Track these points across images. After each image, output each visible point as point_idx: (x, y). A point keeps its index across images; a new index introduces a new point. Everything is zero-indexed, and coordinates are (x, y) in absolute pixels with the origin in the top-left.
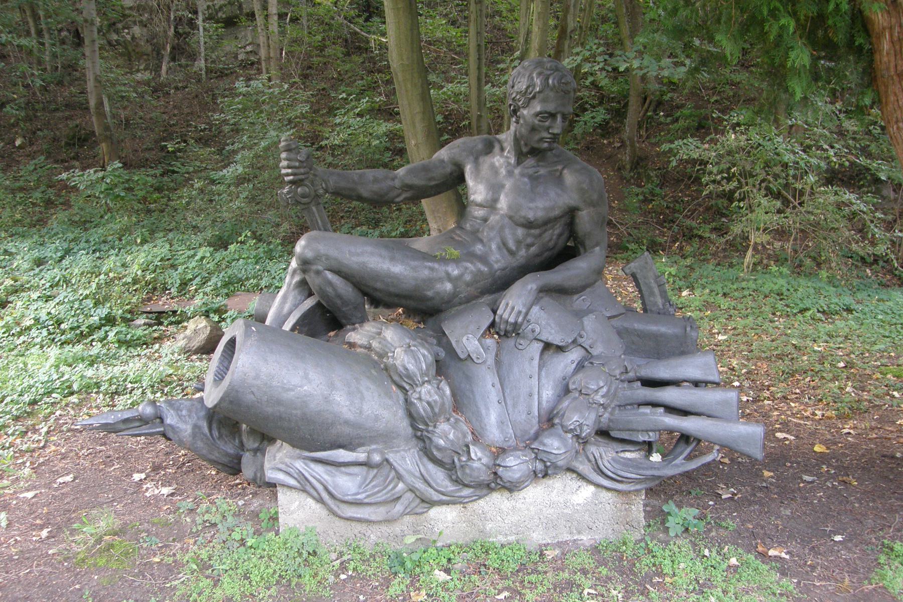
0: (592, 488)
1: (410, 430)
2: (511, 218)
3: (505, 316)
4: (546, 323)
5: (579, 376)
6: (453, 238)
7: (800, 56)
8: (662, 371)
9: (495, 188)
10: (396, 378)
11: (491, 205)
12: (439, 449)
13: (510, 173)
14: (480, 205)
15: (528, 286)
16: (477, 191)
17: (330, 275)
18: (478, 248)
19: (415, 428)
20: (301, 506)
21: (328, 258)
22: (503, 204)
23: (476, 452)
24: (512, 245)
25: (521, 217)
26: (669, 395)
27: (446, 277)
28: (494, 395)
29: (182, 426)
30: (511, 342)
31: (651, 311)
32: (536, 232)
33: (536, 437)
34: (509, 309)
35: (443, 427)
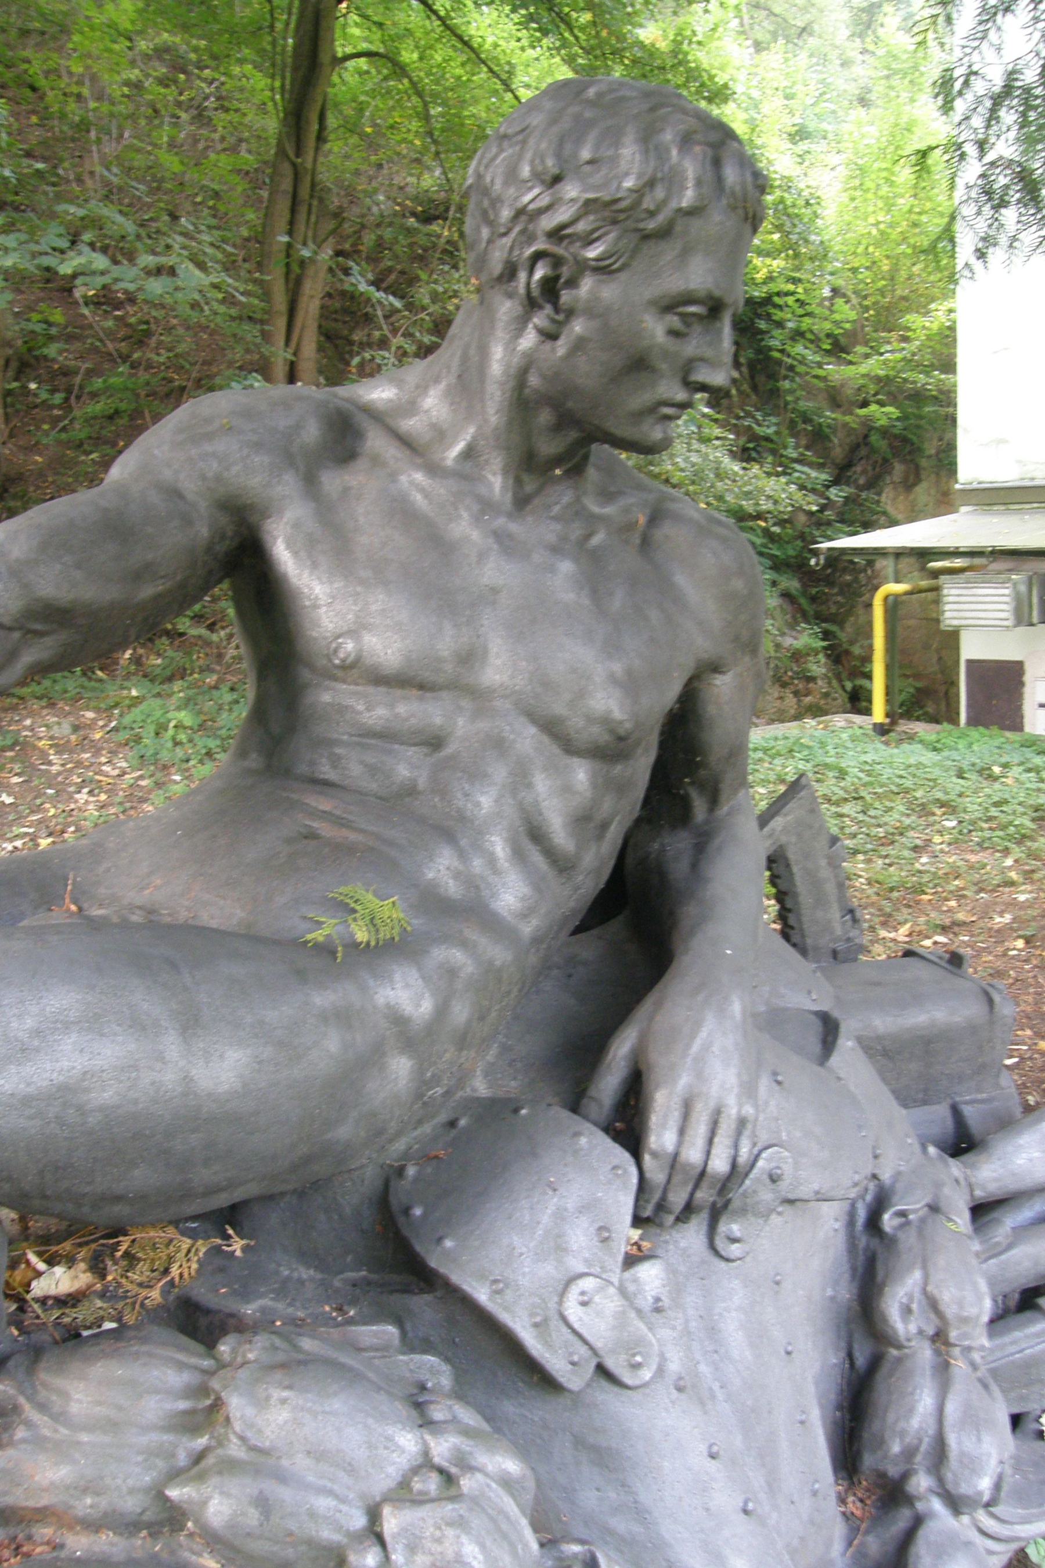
3: (693, 1154)
6: (312, 835)
25: (590, 720)
31: (816, 949)
34: (699, 1130)
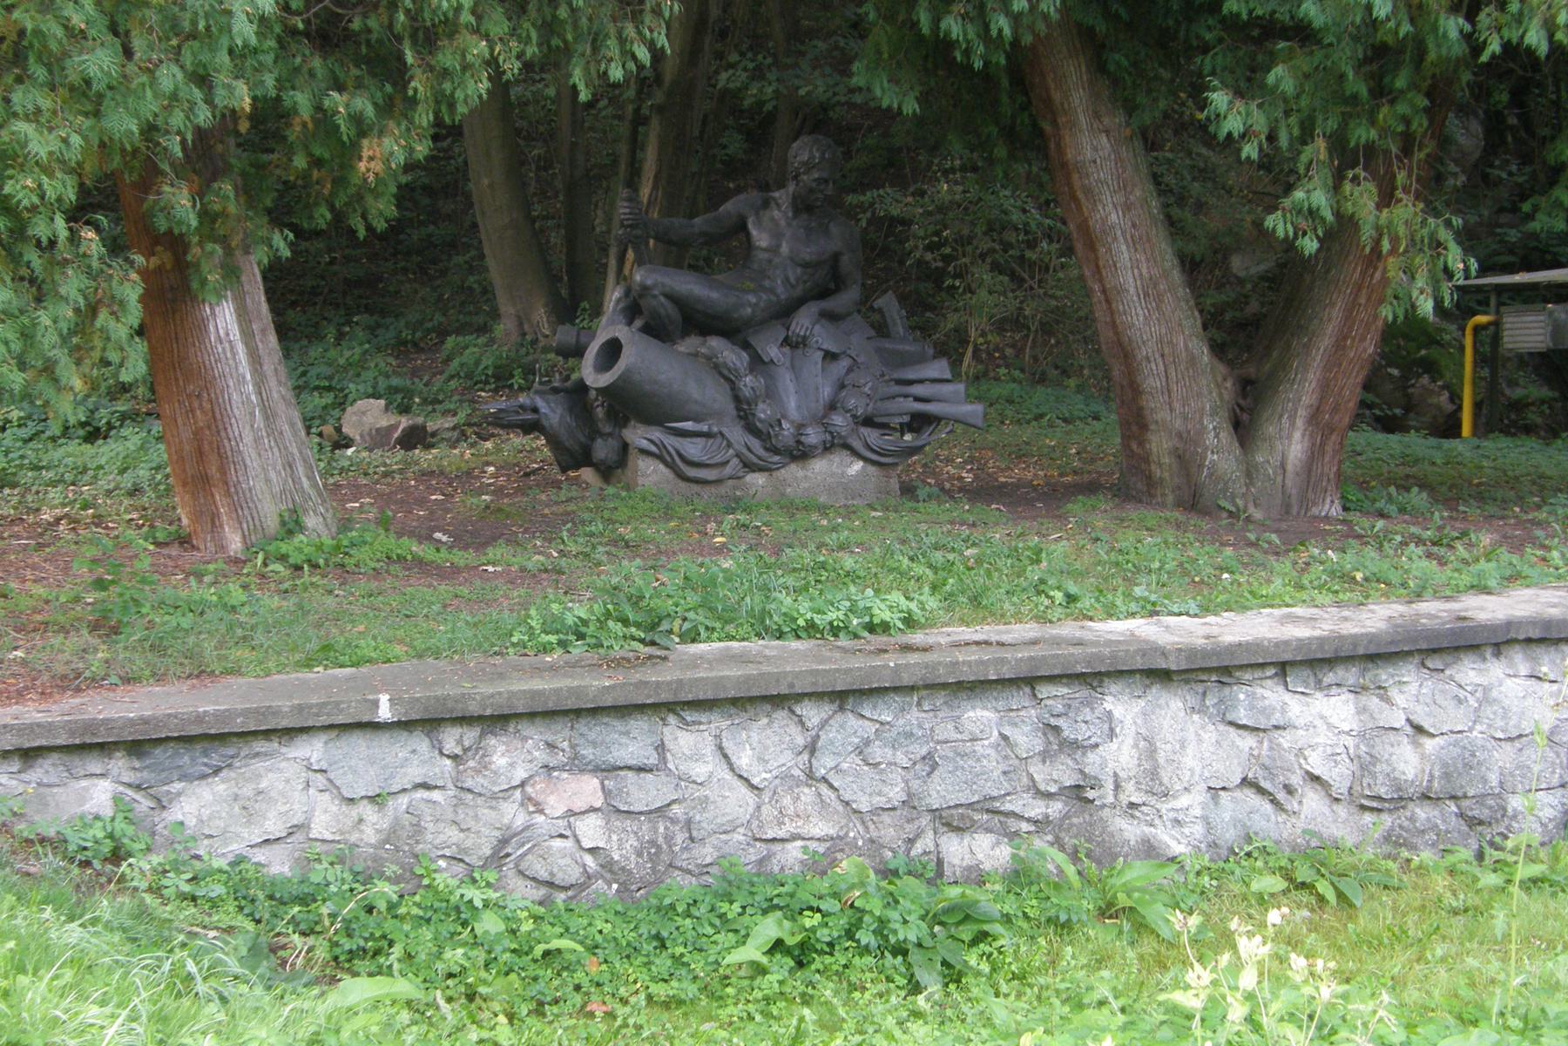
0: (861, 463)
1: (735, 413)
2: (792, 259)
4: (823, 337)
5: (852, 375)
7: (1001, 152)
8: (911, 375)
9: (777, 236)
10: (726, 372)
11: (774, 250)
12: (761, 421)
13: (789, 225)
14: (766, 250)
15: (813, 308)
16: (761, 238)
17: (662, 299)
18: (767, 283)
19: (738, 409)
20: (655, 471)
21: (663, 285)
22: (785, 249)
23: (785, 425)
24: (792, 280)
26: (918, 390)
27: (750, 303)
28: (791, 388)
29: (551, 415)
30: (800, 351)
32: (810, 270)
33: (824, 417)
35: (761, 406)
